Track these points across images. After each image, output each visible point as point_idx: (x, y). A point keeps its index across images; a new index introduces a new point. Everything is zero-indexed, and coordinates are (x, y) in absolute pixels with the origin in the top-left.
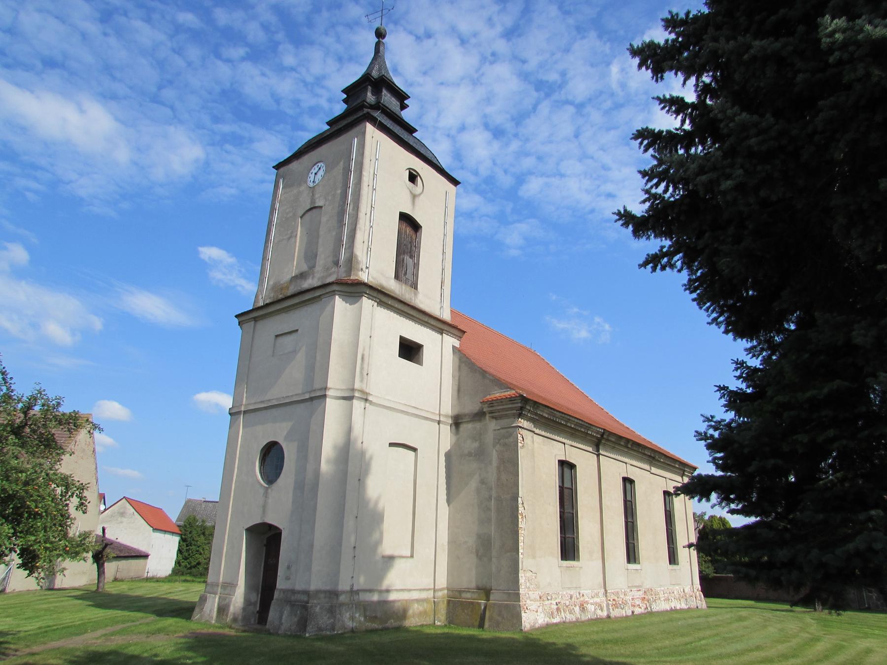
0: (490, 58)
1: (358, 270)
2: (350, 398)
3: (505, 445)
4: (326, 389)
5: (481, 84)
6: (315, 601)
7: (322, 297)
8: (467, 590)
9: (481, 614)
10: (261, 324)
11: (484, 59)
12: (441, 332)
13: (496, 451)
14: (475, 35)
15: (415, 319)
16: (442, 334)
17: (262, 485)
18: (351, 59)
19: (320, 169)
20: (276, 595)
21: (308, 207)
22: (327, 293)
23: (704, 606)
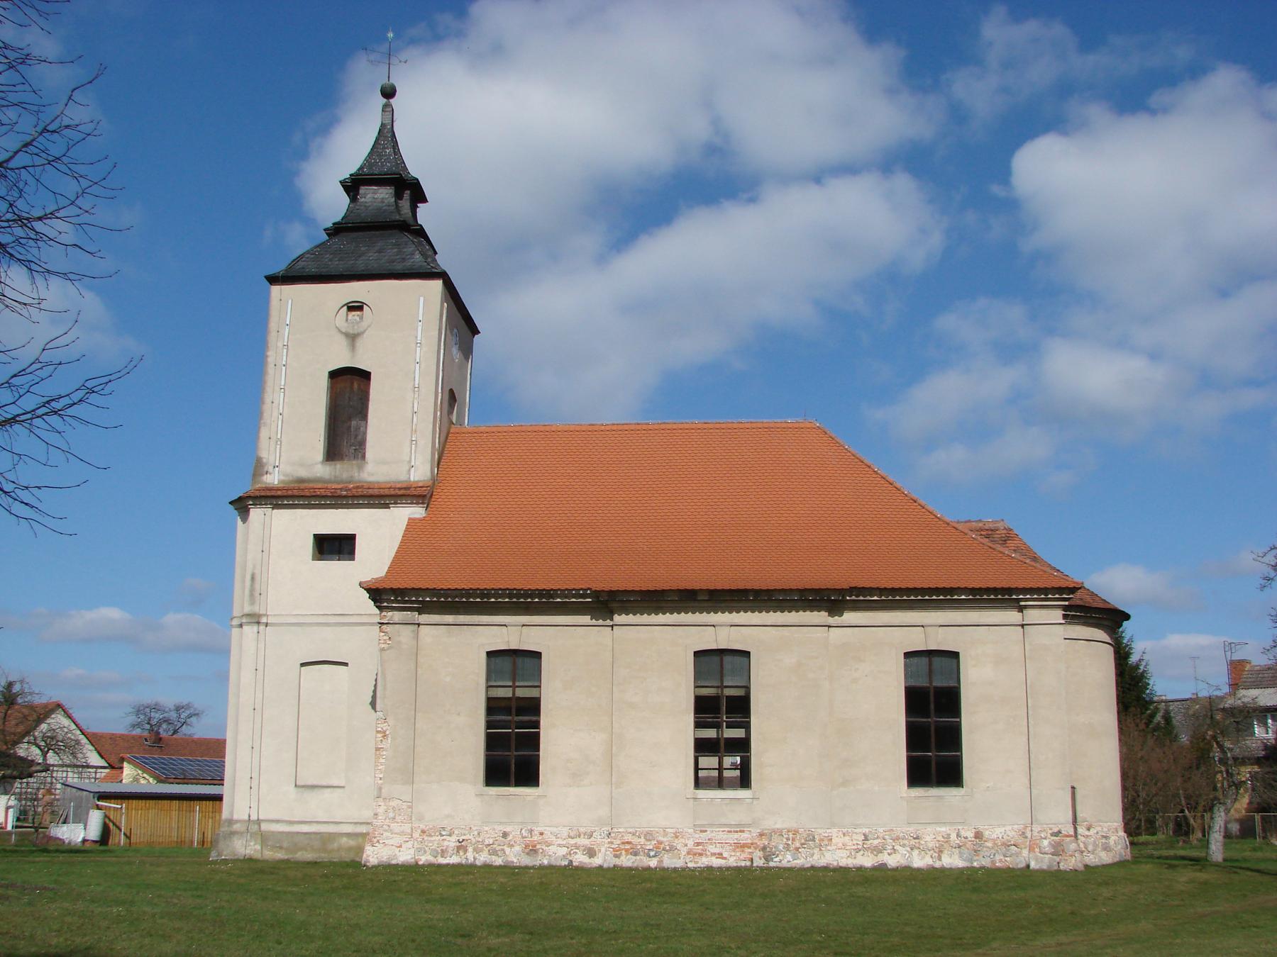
1: (262, 475)
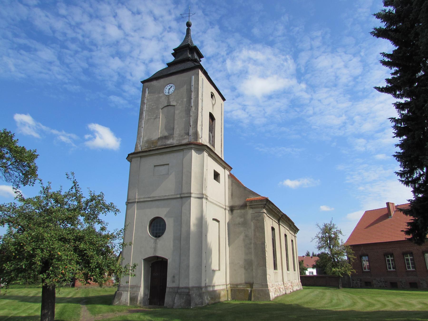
0: (168, 29)
2: (201, 198)
3: (257, 220)
4: (191, 193)
5: (163, 41)
6: (192, 292)
8: (241, 284)
9: (249, 294)
10: (143, 160)
11: (165, 29)
12: (224, 168)
13: (253, 223)
14: (162, 17)
15: (218, 162)
16: (224, 169)
17: (151, 237)
18: (97, 17)
19: (171, 87)
20: (167, 290)
22: (187, 148)
23: (302, 289)
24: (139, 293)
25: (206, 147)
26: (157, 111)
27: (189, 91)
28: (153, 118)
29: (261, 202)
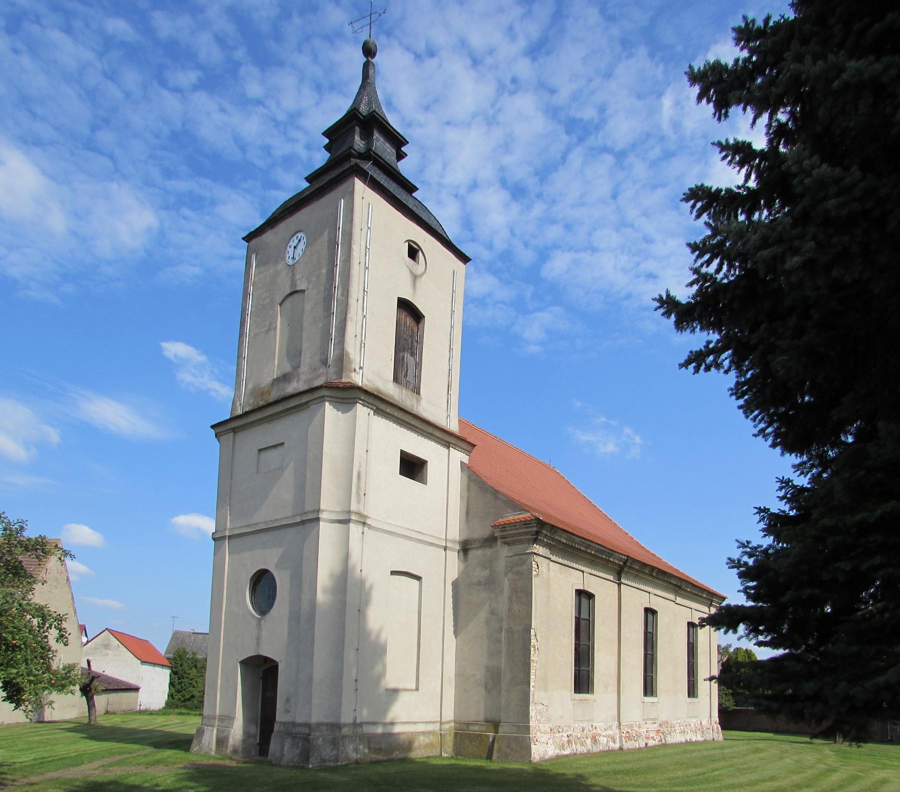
0: (510, 86)
1: (351, 371)
2: (346, 522)
3: (518, 573)
4: (318, 511)
6: (317, 734)
7: (310, 404)
8: (475, 723)
9: (489, 746)
10: (240, 436)
11: (501, 88)
13: (508, 580)
14: (491, 52)
15: (417, 430)
16: (448, 447)
20: (276, 727)
21: (288, 291)
23: (721, 737)
24: (231, 731)
25: (357, 391)
26: (271, 312)
27: (333, 244)
28: (263, 330)
29: (527, 528)
